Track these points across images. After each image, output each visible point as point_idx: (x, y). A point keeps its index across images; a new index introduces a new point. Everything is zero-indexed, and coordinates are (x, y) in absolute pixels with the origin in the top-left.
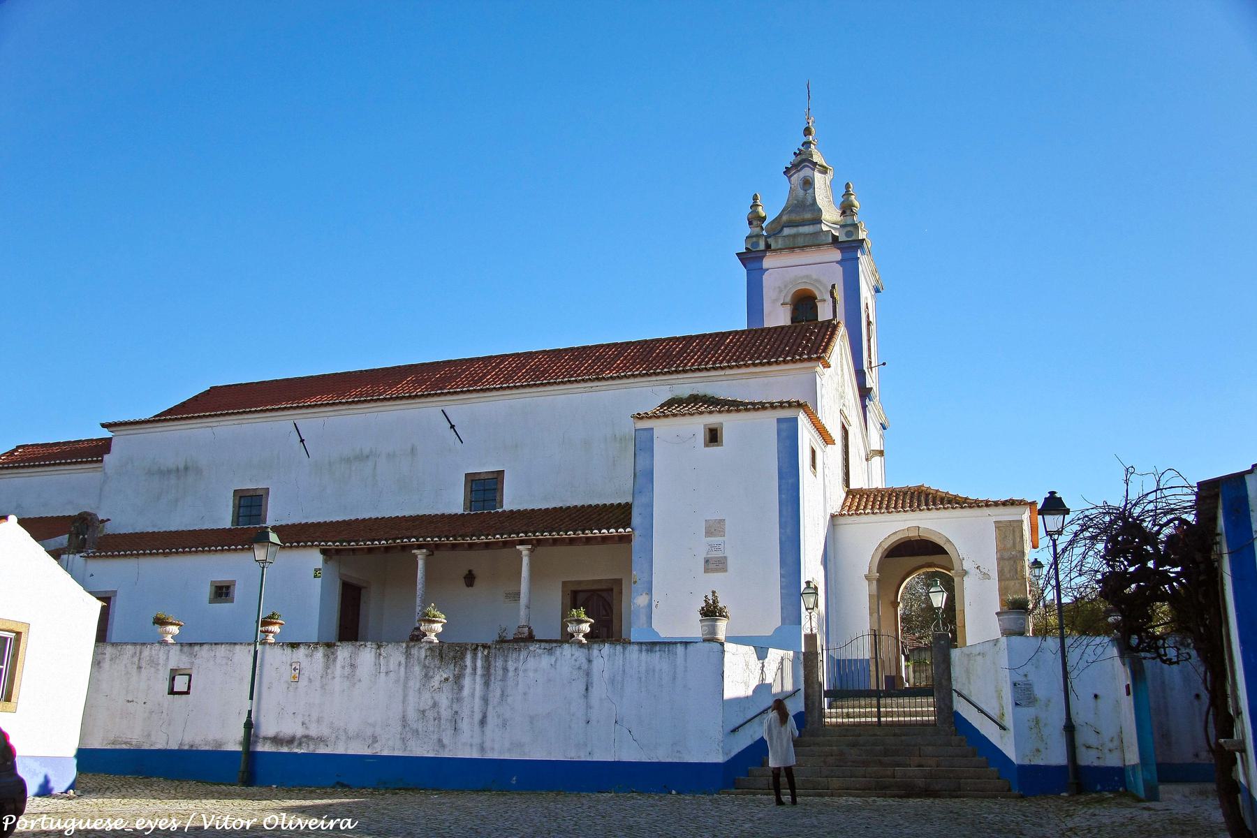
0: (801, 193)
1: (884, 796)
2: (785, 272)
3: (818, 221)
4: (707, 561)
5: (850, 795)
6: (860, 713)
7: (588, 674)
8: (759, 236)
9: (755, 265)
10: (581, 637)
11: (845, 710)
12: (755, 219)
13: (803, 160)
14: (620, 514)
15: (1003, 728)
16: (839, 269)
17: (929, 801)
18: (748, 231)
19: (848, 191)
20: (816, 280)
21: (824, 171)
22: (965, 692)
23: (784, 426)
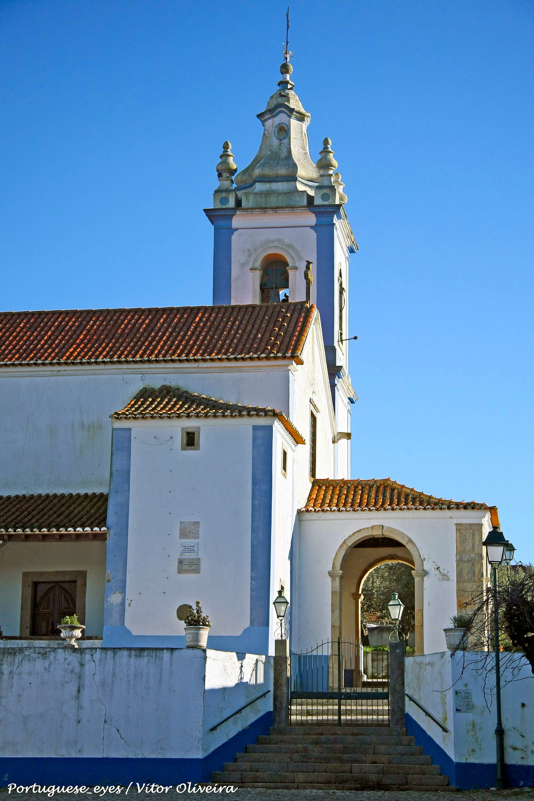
0: (276, 142)
1: (343, 789)
2: (255, 234)
3: (293, 178)
4: (180, 562)
5: (314, 788)
6: (323, 711)
7: (80, 677)
8: (228, 191)
9: (222, 223)
10: (73, 642)
11: (304, 707)
12: (224, 171)
13: (279, 106)
14: (92, 509)
15: (445, 730)
16: (313, 234)
17: (380, 793)
18: (216, 184)
19: (326, 148)
20: (290, 246)
21: (301, 118)
22: (416, 697)
23: (260, 433)
